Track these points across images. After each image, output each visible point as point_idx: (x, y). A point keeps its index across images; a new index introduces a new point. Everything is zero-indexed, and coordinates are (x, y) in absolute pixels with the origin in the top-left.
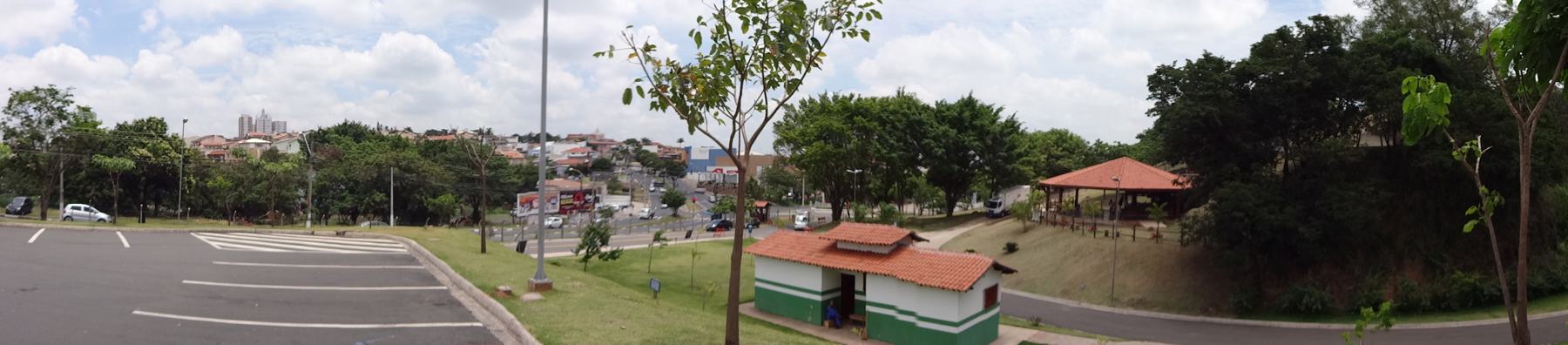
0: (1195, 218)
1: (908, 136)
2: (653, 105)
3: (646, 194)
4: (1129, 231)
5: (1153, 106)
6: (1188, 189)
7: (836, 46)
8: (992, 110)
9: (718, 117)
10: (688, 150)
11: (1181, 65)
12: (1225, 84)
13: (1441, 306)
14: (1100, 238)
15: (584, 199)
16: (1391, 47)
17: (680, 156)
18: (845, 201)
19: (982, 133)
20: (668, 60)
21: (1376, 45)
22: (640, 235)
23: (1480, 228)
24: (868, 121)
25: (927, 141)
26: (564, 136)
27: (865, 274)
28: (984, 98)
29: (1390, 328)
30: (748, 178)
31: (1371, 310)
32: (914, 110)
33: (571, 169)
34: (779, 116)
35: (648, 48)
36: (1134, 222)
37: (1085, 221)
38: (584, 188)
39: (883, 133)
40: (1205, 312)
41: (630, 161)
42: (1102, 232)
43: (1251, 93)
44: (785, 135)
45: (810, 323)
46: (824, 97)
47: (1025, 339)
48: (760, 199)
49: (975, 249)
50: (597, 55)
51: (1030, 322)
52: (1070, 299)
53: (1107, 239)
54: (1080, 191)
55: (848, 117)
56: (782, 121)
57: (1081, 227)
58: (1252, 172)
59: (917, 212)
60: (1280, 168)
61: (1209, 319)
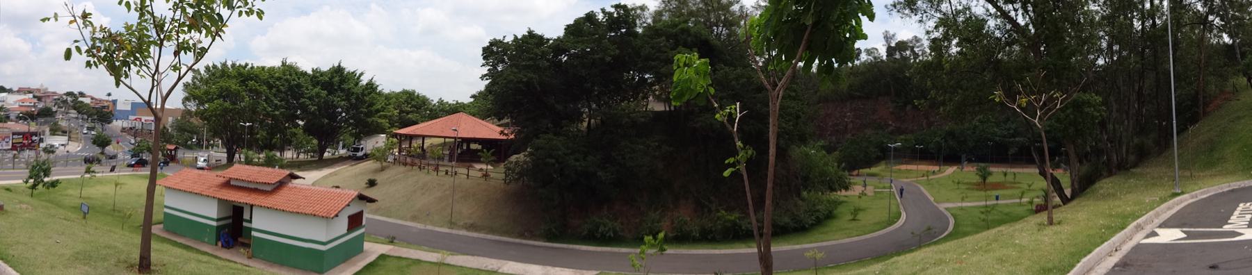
0: (517, 163)
1: (289, 97)
2: (88, 64)
3: (79, 136)
4: (464, 171)
5: (486, 72)
7: (236, 24)
9: (140, 74)
10: (114, 102)
12: (544, 54)
13: (708, 237)
14: (442, 176)
15: (31, 140)
16: (674, 31)
17: (108, 107)
18: (237, 147)
19: (348, 94)
20: (101, 26)
21: (661, 30)
22: (74, 168)
23: (736, 174)
24: (259, 86)
25: (303, 100)
26: (15, 89)
27: (252, 206)
28: (349, 67)
29: (664, 252)
30: (161, 127)
31: (651, 238)
33: (21, 115)
34: (188, 78)
35: (85, 16)
36: (468, 164)
38: (31, 131)
39: (270, 95)
40: (522, 236)
41: (69, 110)
44: (192, 93)
45: (207, 243)
46: (224, 65)
47: (384, 252)
48: (171, 143)
49: (340, 186)
50: (43, 20)
51: (387, 240)
52: (419, 222)
54: (426, 138)
56: (190, 82)
57: (426, 167)
58: (562, 128)
59: (295, 156)
60: (585, 124)
61: (524, 242)
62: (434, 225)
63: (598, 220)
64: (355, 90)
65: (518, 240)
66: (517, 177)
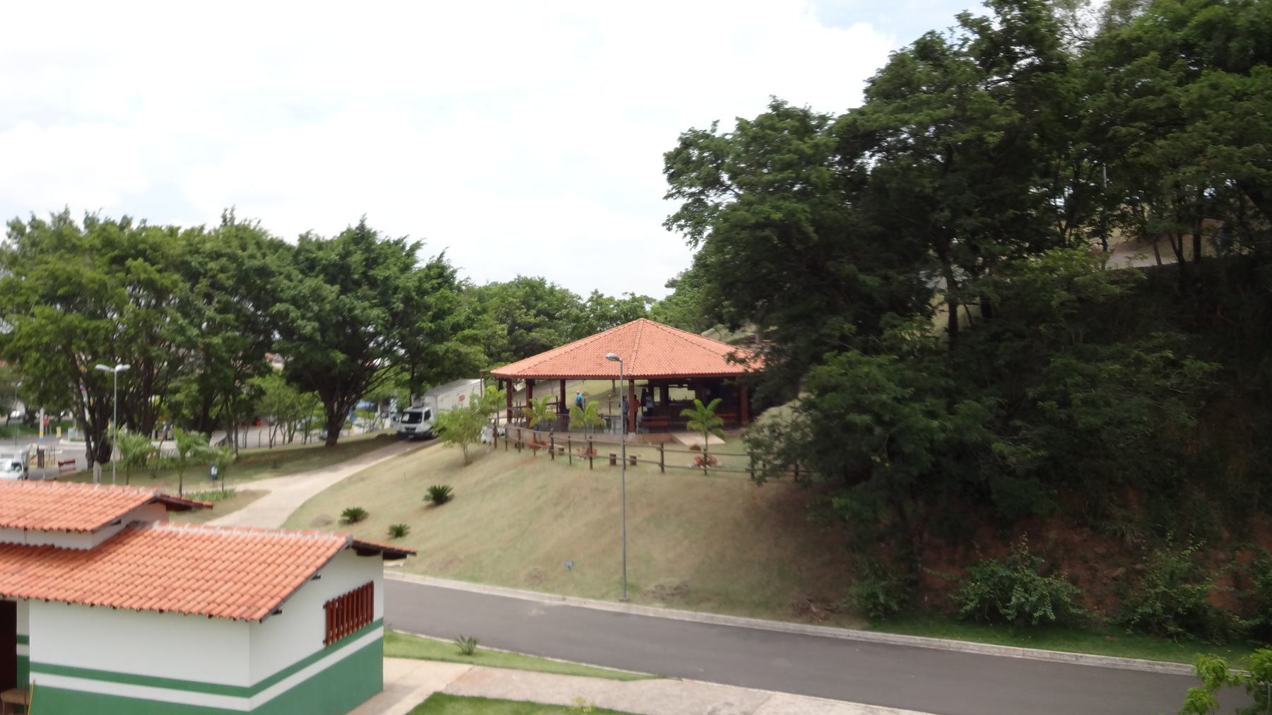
0: (773, 428)
6: (756, 371)
8: (404, 247)
11: (727, 128)
12: (816, 158)
19: (385, 291)
21: (1139, 39)
24: (160, 271)
28: (386, 230)
32: (252, 249)
36: (663, 436)
37: (571, 439)
40: (802, 612)
42: (605, 458)
43: (870, 180)
47: (441, 687)
52: (547, 590)
53: (613, 468)
55: (114, 260)
57: (567, 451)
58: (881, 332)
59: (279, 438)
60: (941, 320)
61: (811, 629)
62: (584, 594)
63: (1003, 572)
64: (402, 281)
65: (793, 626)
66: (778, 462)
